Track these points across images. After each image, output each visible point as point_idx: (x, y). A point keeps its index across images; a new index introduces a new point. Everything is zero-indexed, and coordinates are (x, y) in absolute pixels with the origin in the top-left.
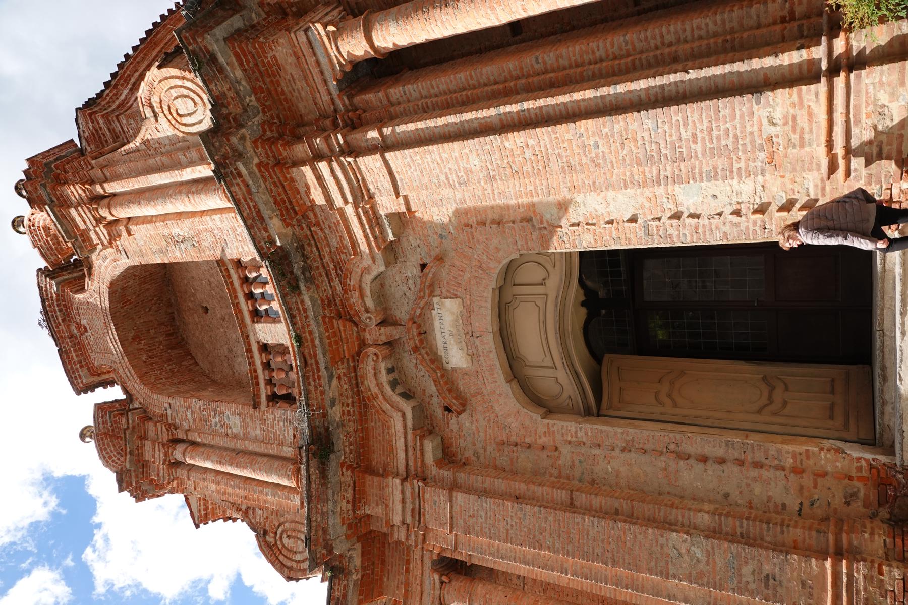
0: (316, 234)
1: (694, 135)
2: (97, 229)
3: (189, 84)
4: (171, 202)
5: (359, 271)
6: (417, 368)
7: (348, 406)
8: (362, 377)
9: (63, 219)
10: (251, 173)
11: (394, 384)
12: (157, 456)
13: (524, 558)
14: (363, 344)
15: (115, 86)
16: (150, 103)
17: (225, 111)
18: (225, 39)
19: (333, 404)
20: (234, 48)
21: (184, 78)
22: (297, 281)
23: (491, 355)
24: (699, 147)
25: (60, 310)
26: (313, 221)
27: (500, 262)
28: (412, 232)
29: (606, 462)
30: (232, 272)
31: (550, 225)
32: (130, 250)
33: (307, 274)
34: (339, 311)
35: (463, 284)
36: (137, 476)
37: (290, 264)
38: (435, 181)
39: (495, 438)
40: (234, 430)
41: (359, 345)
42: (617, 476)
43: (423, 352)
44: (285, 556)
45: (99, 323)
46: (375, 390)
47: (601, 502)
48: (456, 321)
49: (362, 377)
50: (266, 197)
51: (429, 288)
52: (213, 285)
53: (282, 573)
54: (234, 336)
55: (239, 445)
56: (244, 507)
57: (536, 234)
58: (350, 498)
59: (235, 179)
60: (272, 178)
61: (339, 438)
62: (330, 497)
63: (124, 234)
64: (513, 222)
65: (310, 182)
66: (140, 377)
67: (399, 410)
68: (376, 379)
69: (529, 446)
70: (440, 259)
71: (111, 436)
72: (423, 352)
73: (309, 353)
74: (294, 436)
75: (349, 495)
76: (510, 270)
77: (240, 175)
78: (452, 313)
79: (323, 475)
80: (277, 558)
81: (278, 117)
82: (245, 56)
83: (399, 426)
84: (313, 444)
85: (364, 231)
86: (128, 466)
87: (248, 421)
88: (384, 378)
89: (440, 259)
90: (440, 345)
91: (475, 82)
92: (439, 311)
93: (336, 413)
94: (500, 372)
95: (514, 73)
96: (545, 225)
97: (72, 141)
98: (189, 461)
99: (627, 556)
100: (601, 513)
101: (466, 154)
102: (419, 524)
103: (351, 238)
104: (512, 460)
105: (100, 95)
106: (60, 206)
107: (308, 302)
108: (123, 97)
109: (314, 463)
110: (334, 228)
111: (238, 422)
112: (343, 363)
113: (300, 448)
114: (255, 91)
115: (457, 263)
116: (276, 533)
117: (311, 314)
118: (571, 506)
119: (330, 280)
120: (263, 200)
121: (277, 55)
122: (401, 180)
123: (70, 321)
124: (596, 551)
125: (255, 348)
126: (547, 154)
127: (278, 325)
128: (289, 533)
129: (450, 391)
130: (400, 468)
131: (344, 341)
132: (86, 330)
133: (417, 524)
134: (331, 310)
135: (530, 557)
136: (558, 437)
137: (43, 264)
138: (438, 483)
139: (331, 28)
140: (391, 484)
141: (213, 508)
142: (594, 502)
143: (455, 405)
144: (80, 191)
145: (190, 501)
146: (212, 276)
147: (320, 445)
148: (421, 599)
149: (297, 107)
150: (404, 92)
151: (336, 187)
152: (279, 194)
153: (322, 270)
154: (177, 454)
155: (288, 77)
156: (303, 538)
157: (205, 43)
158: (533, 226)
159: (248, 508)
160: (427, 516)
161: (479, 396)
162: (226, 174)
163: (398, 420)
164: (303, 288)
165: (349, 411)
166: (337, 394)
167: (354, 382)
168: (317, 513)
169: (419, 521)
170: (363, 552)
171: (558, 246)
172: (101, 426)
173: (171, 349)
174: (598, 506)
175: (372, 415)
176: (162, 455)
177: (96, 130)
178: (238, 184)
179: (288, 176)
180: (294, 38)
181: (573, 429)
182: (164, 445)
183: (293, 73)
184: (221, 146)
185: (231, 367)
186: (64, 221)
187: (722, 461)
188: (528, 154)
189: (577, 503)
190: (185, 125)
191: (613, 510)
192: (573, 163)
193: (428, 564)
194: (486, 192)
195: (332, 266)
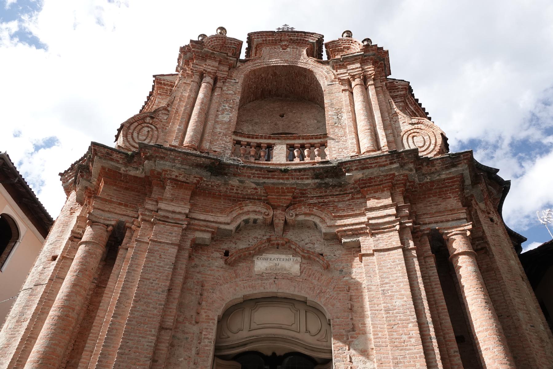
0: (347, 196)
2: (347, 74)
3: (432, 147)
4: (365, 119)
5: (323, 216)
6: (255, 238)
7: (237, 190)
8: (255, 203)
9: (354, 59)
10: (391, 169)
11: (246, 221)
12: (209, 67)
13: (127, 288)
14: (274, 208)
15: (415, 104)
16: (420, 123)
17: (425, 164)
18: (462, 174)
19: (241, 182)
20: (457, 177)
21: (435, 145)
22: (321, 179)
23: (262, 288)
25: (297, 40)
26: (356, 196)
27: (324, 305)
28: (344, 253)
29: (186, 358)
30: (319, 141)
31: (350, 342)
32: (333, 88)
33: (324, 185)
34: (297, 199)
35: (310, 279)
36: (197, 52)
37: (332, 177)
38: (384, 276)
39: (206, 281)
40: (220, 116)
41: (274, 205)
42: (175, 364)
43: (267, 244)
44: (136, 127)
45: (287, 57)
46: (246, 209)
47: (163, 350)
48: (285, 270)
49: (255, 203)
50: (375, 174)
51: (308, 257)
52: (297, 124)
53: (127, 122)
54: (265, 128)
55: (211, 117)
56: (169, 109)
57: (344, 332)
58: (178, 178)
59: (390, 160)
60: (386, 180)
61: (218, 180)
62: (184, 167)
63: (343, 88)
64: (352, 319)
65: (381, 200)
66: (254, 71)
67: (232, 221)
68: (252, 211)
69: (200, 304)
70: (327, 267)
71: (223, 45)
72: (267, 244)
73: (274, 175)
74: (215, 151)
75: (181, 178)
76: (317, 310)
77: (391, 163)
78: (290, 268)
79: (198, 166)
80: (136, 121)
81: (415, 191)
82: (452, 182)
83: (222, 219)
84: (219, 164)
85: (349, 225)
86: (206, 49)
87: (226, 126)
88: (252, 216)
89: (327, 267)
91: (440, 310)
92: (292, 260)
93: (234, 182)
94: (251, 293)
95: (447, 336)
96: (350, 339)
97: (390, 74)
98: (203, 85)
99: (125, 364)
100: (156, 349)
101: (403, 298)
102: (158, 220)
103: (345, 216)
104: (191, 290)
105: (413, 95)
106: (362, 59)
107: (307, 182)
108: (411, 107)
109: (208, 161)
110: (350, 207)
111: (225, 119)
112: (264, 193)
113: (208, 153)
114: (432, 182)
115: (323, 278)
116: (151, 124)
117: (299, 182)
118: (162, 328)
119: (318, 197)
120: (375, 172)
121: (451, 199)
122: (384, 255)
123: (290, 42)
124: (130, 342)
125: (270, 141)
126: (405, 349)
127: (285, 159)
128: (151, 133)
129: (240, 257)
130: (194, 214)
131: (279, 197)
132: (283, 49)
133: (159, 218)
134: (298, 194)
135: (127, 292)
136: (205, 325)
137: (326, 40)
138: (183, 236)
140: (186, 206)
141: (164, 88)
142: (163, 345)
143: (231, 259)
144: (370, 72)
145: (171, 77)
146: (303, 125)
147: (217, 168)
148: (99, 209)
149: (421, 203)
150: (432, 267)
151: (379, 215)
152: (375, 182)
153: (324, 194)
154: (208, 79)
155: (439, 202)
156: (146, 142)
157: (463, 164)
158: (349, 331)
159: (168, 111)
160: (162, 226)
161: (234, 275)
162: (393, 156)
163: (225, 219)
164: (316, 181)
165: (233, 189)
166: (246, 185)
167: (251, 197)
168: (176, 156)
169: (160, 220)
170: (137, 177)
171: (336, 345)
172: (230, 41)
173: (262, 91)
174: (160, 348)
175: (228, 203)
176: (209, 70)
177: (397, 89)
178: (386, 161)
179: (385, 189)
180: (462, 211)
181: (210, 337)
182: (216, 73)
183: (441, 206)
184: (409, 158)
185: (246, 121)
186: (353, 59)
188: (405, 337)
189: (163, 332)
190: (407, 138)
191: (156, 359)
192: (400, 365)
193: (124, 219)
194: (376, 306)
195: (326, 200)
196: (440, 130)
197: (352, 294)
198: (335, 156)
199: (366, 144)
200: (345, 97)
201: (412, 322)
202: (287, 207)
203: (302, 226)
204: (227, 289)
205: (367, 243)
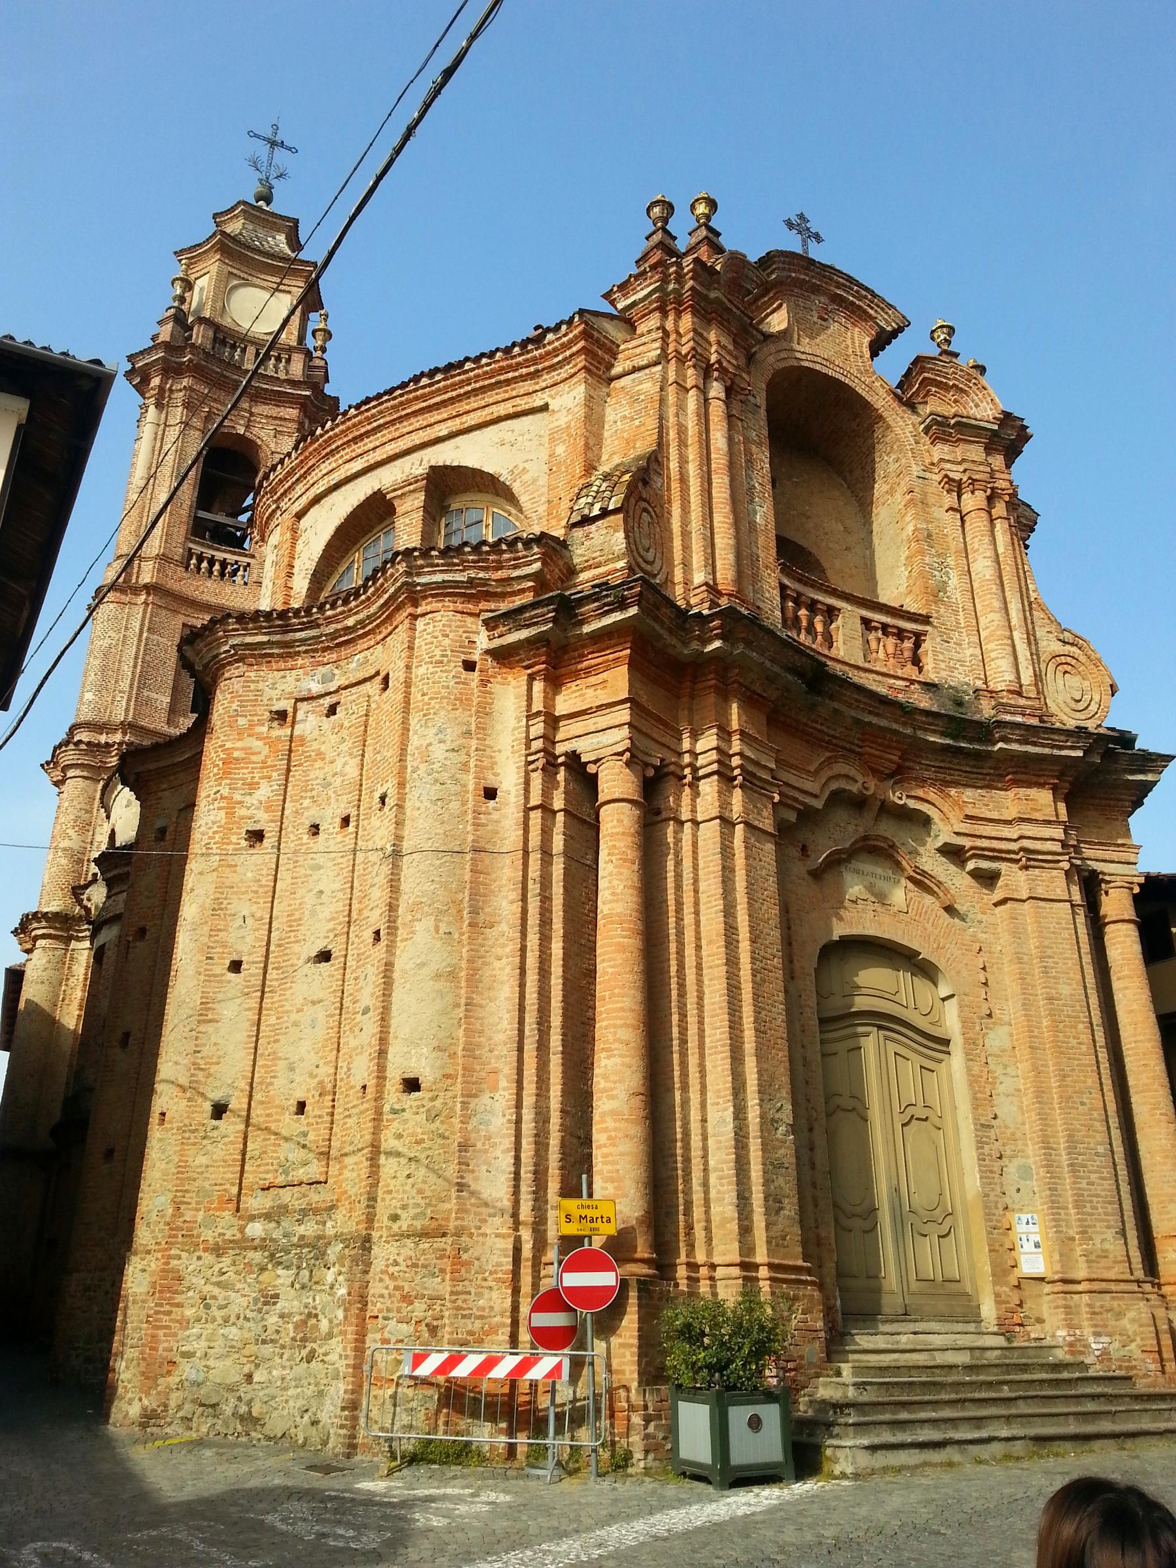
1: (1092, 1184)
24: (1084, 1185)
75: (757, 688)
83: (809, 786)
90: (861, 866)
158: (982, 1018)
196: (1111, 678)
198: (944, 674)
201: (1083, 1022)
202: (891, 776)
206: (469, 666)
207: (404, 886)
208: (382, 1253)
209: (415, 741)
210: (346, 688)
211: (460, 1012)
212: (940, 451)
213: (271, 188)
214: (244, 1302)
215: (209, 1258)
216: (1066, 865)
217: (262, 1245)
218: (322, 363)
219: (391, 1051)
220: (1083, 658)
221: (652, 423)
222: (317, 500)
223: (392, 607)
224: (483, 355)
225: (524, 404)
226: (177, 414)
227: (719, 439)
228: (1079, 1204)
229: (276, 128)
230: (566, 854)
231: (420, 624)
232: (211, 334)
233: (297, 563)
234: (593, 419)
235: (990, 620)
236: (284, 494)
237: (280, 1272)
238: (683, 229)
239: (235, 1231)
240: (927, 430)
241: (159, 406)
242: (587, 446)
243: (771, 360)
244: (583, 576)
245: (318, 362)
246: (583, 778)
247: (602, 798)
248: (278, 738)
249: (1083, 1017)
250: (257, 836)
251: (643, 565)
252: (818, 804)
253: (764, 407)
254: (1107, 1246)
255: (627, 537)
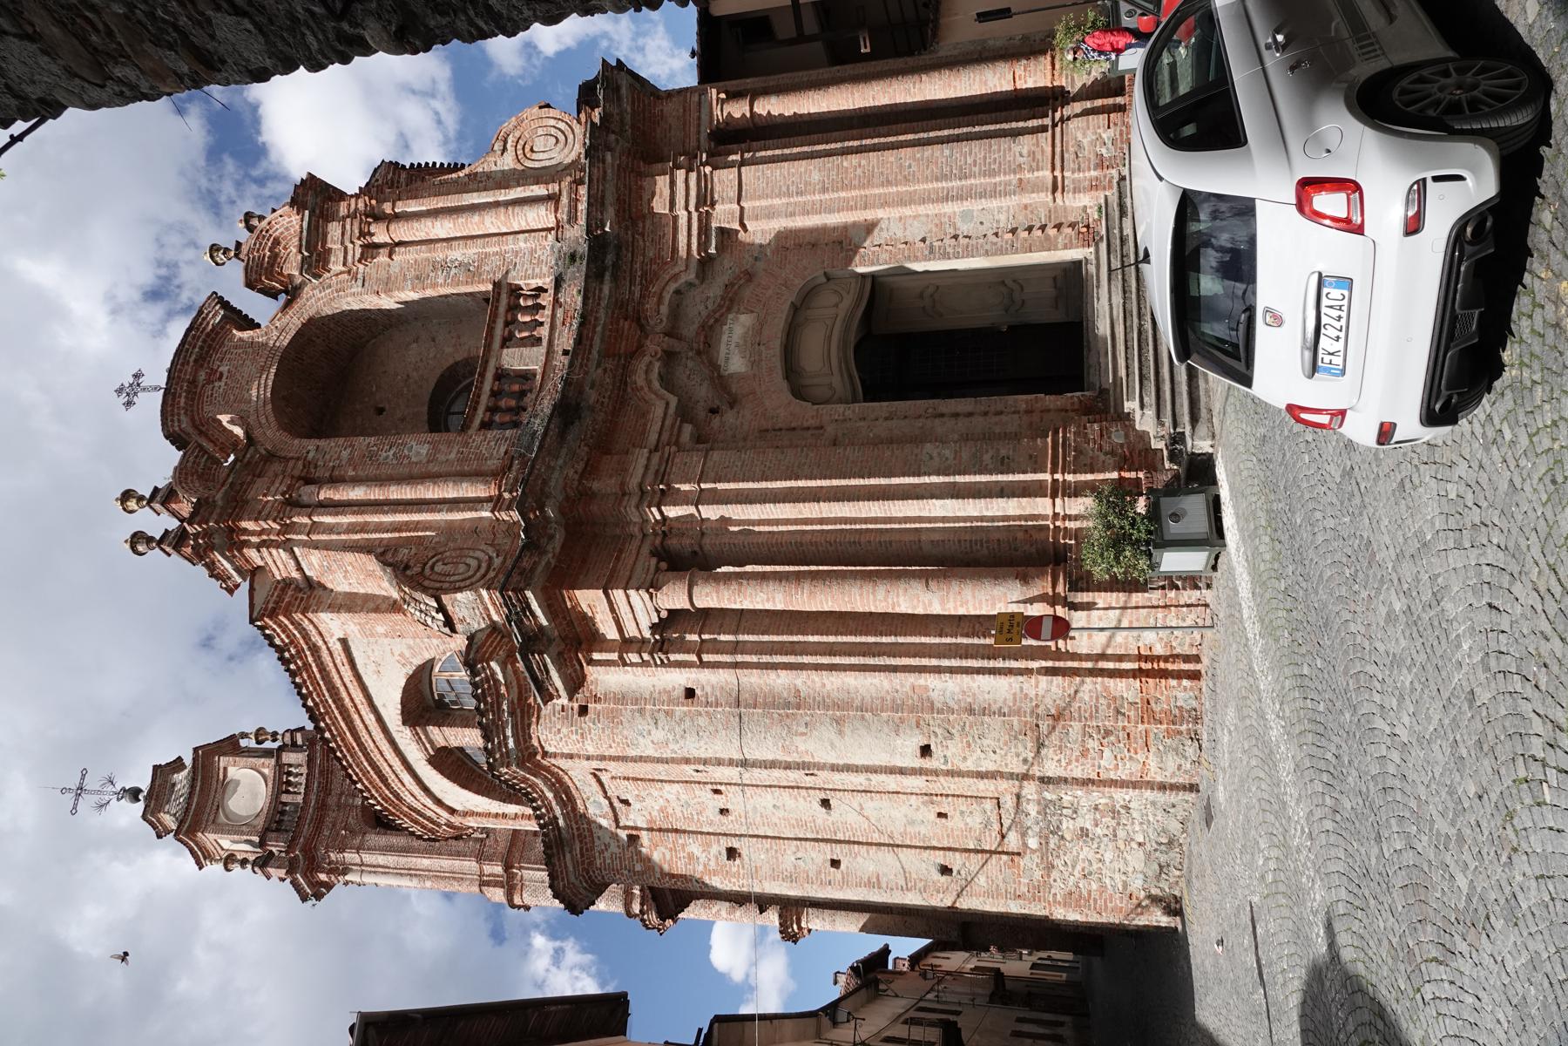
34: (631, 314)
36: (220, 515)
37: (605, 254)
46: (641, 382)
51: (731, 301)
75: (580, 467)
79: (562, 436)
83: (659, 411)
86: (220, 495)
90: (722, 355)
93: (592, 396)
114: (633, 127)
117: (604, 303)
125: (489, 375)
139: (723, 96)
146: (416, 369)
186: (313, 233)
187: (970, 414)
188: (859, 171)
197: (789, 243)
198: (545, 269)
199: (541, 216)
200: (401, 256)
202: (642, 328)
203: (676, 312)
204: (777, 401)
205: (724, 214)
206: (583, 710)
207: (770, 757)
208: (1051, 769)
209: (650, 752)
210: (605, 792)
211: (868, 715)
212: (336, 266)
213: (124, 789)
214: (1086, 849)
215: (1055, 874)
216: (708, 169)
217: (1044, 840)
218: (288, 735)
219: (900, 764)
220: (517, 134)
221: (349, 557)
222: (439, 802)
223: (538, 769)
224: (299, 693)
225: (340, 657)
226: (350, 857)
227: (357, 493)
228: (992, 173)
229: (64, 791)
230: (735, 633)
231: (547, 748)
232: (274, 835)
233: (494, 811)
234: (352, 604)
235: (491, 223)
236: (433, 822)
237: (1064, 826)
238: (158, 523)
239: (1034, 857)
240: (317, 276)
241: (345, 872)
242: (377, 610)
243: (272, 435)
244: (495, 618)
245: (288, 739)
246: (670, 622)
247: (687, 606)
248: (651, 840)
249: (837, 160)
250: (732, 853)
251: (482, 571)
252: (673, 401)
253: (317, 442)
254: (1025, 152)
255: (460, 590)
